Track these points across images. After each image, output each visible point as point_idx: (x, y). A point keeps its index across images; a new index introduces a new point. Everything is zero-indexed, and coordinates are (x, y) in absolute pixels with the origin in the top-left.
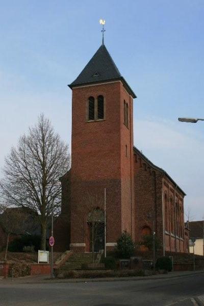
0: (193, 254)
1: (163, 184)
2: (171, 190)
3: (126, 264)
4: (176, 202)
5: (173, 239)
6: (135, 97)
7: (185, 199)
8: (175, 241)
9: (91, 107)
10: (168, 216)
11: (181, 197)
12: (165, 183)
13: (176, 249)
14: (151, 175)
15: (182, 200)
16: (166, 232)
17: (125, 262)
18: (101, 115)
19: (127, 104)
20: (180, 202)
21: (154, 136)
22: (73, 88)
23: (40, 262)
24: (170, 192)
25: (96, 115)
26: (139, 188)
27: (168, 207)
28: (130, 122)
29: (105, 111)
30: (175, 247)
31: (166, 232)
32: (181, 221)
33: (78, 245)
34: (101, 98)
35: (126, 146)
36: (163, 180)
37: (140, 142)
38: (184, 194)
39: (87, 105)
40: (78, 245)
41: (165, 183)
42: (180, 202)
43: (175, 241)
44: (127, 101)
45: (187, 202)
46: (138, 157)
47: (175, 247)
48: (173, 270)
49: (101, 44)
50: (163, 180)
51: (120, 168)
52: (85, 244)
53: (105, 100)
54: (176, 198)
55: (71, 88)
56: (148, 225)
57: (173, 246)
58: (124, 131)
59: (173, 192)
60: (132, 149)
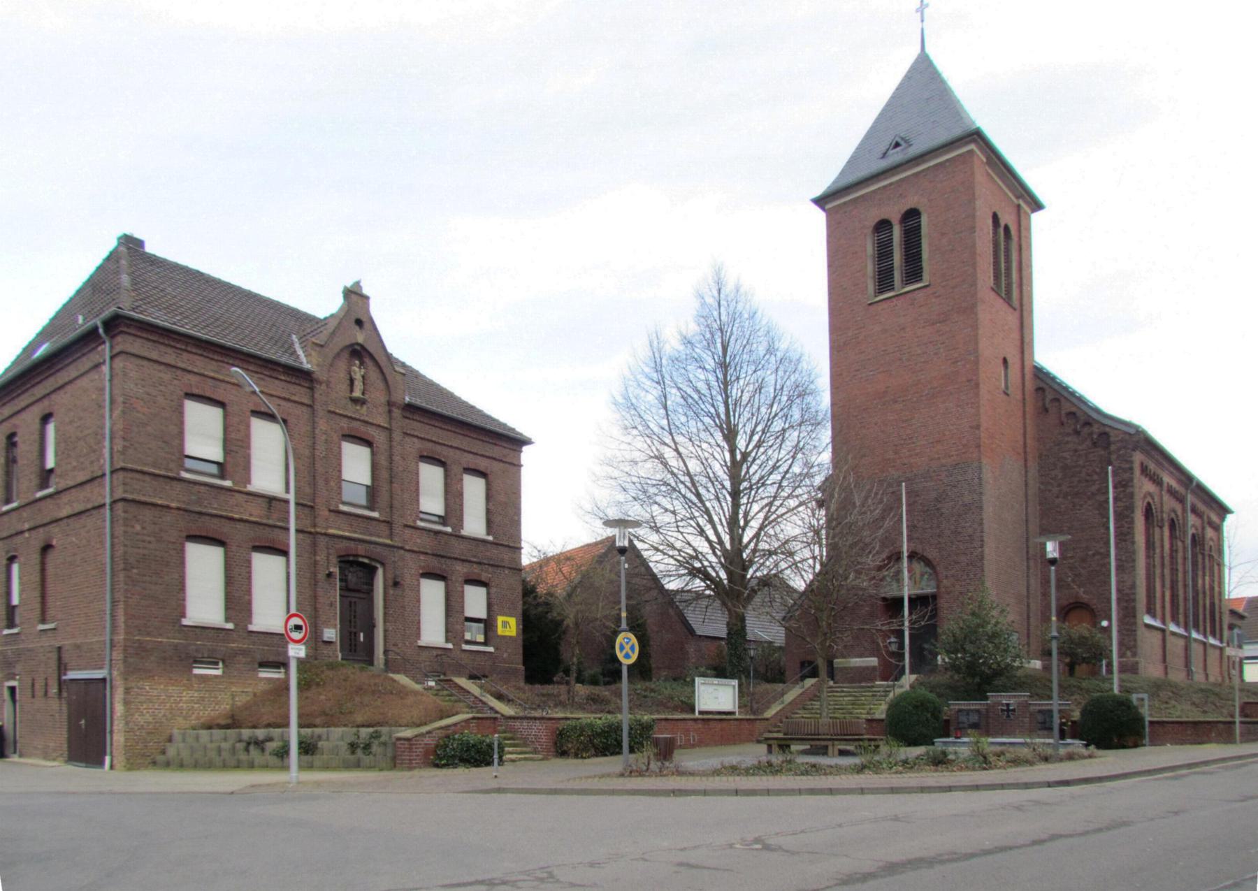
0: (810, 586)
1: (1137, 472)
2: (1171, 491)
3: (974, 718)
4: (1191, 531)
5: (1176, 646)
6: (1037, 206)
7: (1229, 523)
8: (1187, 649)
9: (884, 252)
10: (1158, 571)
11: (1214, 518)
12: (1144, 470)
13: (1189, 673)
14: (1095, 444)
15: (1218, 529)
16: (1148, 620)
17: (968, 712)
18: (914, 271)
19: (1007, 228)
20: (1210, 533)
23: (700, 713)
24: (1166, 497)
25: (897, 276)
26: (1055, 490)
27: (1158, 544)
28: (1021, 285)
29: (925, 255)
30: (1187, 663)
31: (1148, 620)
32: (1212, 588)
33: (856, 662)
34: (912, 216)
35: (1005, 361)
36: (1138, 457)
37: (1062, 352)
38: (1223, 510)
39: (870, 248)
40: (856, 662)
41: (1144, 470)
42: (1210, 533)
43: (1187, 649)
44: (1007, 218)
45: (1237, 536)
46: (1049, 396)
47: (1187, 663)
48: (1147, 740)
49: (915, 52)
50: (1138, 457)
51: (978, 427)
52: (875, 659)
54: (1192, 519)
55: (823, 209)
56: (1085, 597)
57: (1176, 660)
59: (1181, 500)
60: (1028, 376)
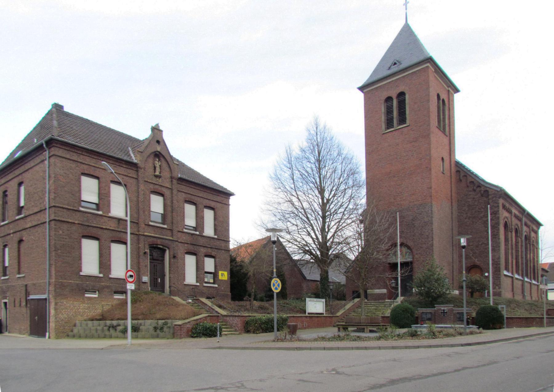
1: (501, 207)
2: (516, 216)
3: (429, 316)
4: (524, 234)
5: (518, 284)
6: (457, 91)
7: (541, 230)
8: (523, 285)
9: (389, 111)
10: (510, 251)
11: (535, 228)
12: (504, 207)
13: (524, 296)
14: (482, 195)
15: (536, 233)
16: (505, 273)
17: (426, 313)
18: (402, 119)
19: (443, 100)
20: (533, 234)
21: (486, 143)
22: (364, 91)
23: (308, 314)
24: (514, 219)
25: (395, 121)
26: (465, 216)
27: (510, 239)
28: (449, 126)
29: (407, 112)
30: (523, 292)
31: (505, 273)
32: (534, 259)
33: (377, 291)
34: (401, 95)
35: (443, 159)
36: (501, 201)
37: (468, 155)
38: (539, 225)
39: (383, 109)
40: (377, 291)
41: (504, 207)
42: (533, 234)
43: (523, 285)
44: (443, 96)
45: (545, 236)
46: (462, 174)
47: (523, 292)
48: (505, 326)
49: (403, 23)
50: (501, 201)
51: (431, 188)
52: (385, 290)
53: (407, 97)
54: (525, 228)
55: (362, 92)
56: (478, 263)
57: (518, 290)
58: (436, 136)
59: (520, 220)
60: (453, 166)
